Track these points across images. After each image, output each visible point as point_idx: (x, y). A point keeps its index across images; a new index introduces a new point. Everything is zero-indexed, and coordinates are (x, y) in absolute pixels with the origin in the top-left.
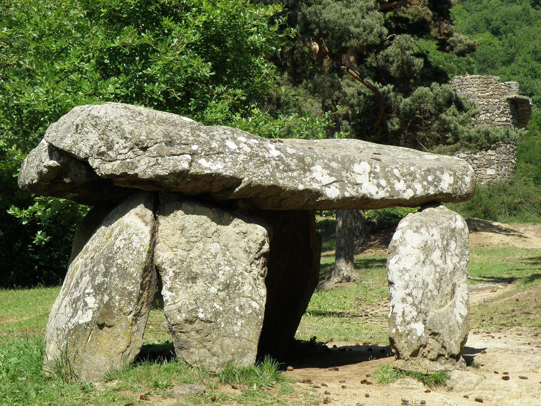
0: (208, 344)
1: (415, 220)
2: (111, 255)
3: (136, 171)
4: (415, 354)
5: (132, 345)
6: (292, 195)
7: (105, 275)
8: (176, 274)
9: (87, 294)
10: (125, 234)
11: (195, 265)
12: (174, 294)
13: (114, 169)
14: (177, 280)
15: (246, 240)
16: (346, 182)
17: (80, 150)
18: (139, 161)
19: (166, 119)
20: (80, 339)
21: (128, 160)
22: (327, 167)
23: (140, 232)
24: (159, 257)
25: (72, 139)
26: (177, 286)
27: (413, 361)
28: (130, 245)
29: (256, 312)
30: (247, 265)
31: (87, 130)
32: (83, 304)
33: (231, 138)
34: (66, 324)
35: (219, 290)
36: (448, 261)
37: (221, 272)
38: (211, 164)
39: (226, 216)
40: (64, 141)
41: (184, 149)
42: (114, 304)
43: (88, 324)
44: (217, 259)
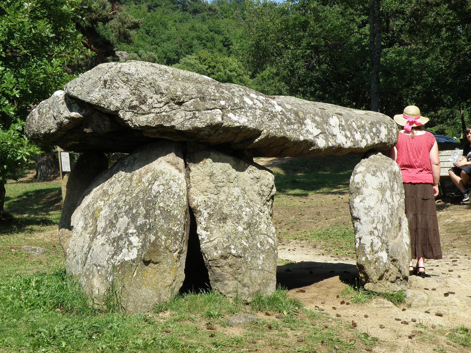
0: (240, 277)
1: (371, 166)
2: (150, 198)
3: (173, 123)
4: (381, 278)
5: (177, 280)
6: (294, 145)
7: (146, 217)
8: (210, 215)
9: (131, 233)
10: (162, 180)
11: (225, 207)
12: (209, 233)
13: (149, 121)
14: (211, 221)
15: (258, 184)
16: (327, 133)
17: (110, 104)
18: (175, 114)
19: (189, 77)
20: (126, 275)
21: (164, 113)
22: (314, 121)
23: (176, 178)
24: (194, 200)
25: (100, 94)
26: (211, 226)
27: (379, 284)
28: (169, 190)
29: (272, 247)
30: (261, 206)
31: (118, 86)
32: (127, 243)
33: (246, 94)
34: (107, 261)
35: (244, 229)
36: (395, 199)
37: (244, 213)
38: (238, 117)
39: (242, 163)
40: (92, 95)
41: (215, 104)
42: (160, 243)
43: (133, 261)
44: (240, 201)
